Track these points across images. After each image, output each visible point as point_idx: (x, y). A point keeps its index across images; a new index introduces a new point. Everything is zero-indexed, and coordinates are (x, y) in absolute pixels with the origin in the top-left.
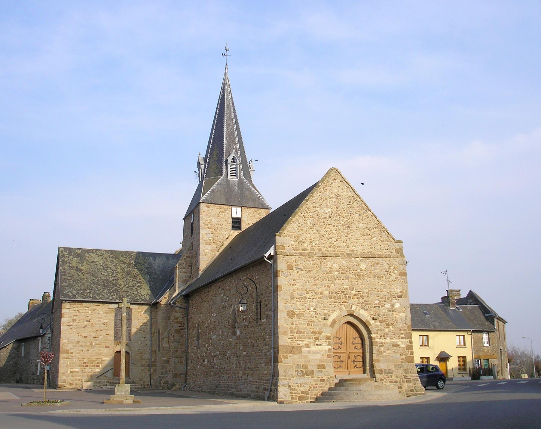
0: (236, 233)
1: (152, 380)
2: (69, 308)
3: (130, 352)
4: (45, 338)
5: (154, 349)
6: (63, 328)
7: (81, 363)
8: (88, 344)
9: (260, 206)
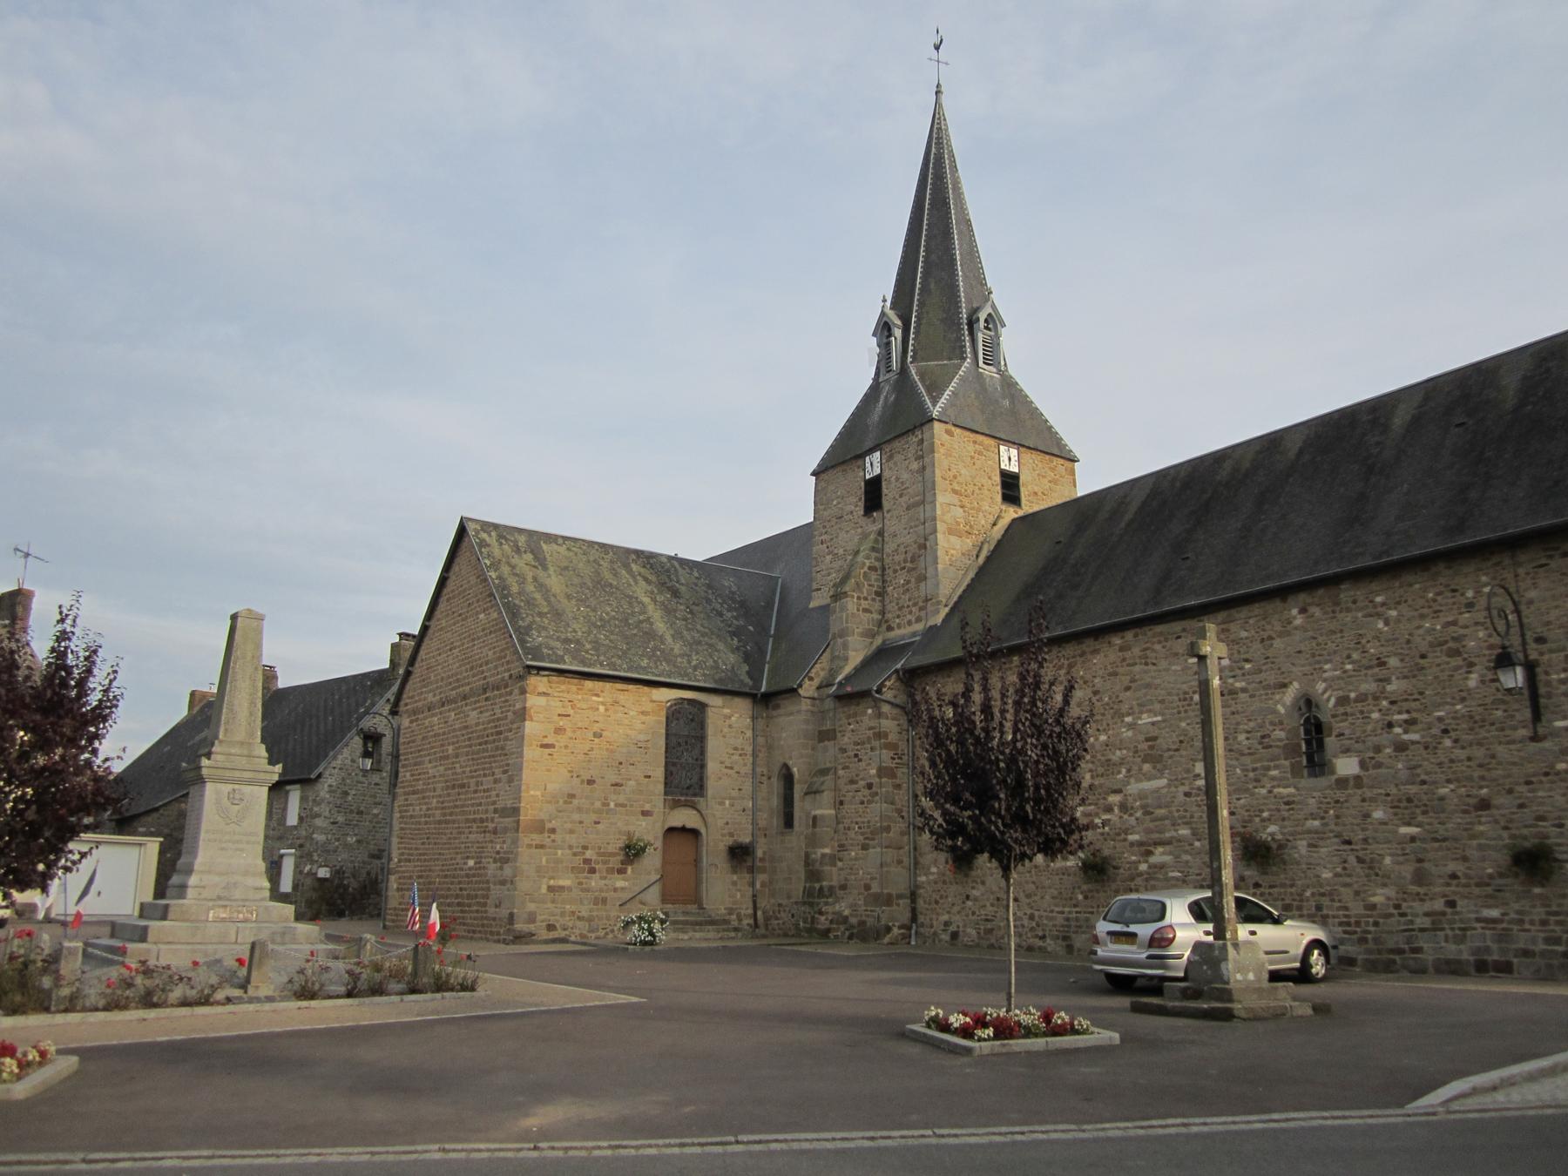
0: (1011, 513)
1: (759, 913)
2: (545, 694)
3: (703, 831)
4: (318, 786)
5: (762, 823)
6: (531, 753)
7: (578, 860)
8: (598, 804)
9: (1056, 451)
